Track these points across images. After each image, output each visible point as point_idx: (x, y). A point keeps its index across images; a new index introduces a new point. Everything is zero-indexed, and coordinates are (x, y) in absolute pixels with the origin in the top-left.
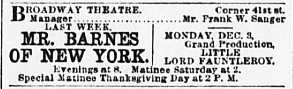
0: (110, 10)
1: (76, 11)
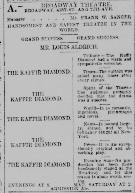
0: (84, 18)
1: (51, 11)
